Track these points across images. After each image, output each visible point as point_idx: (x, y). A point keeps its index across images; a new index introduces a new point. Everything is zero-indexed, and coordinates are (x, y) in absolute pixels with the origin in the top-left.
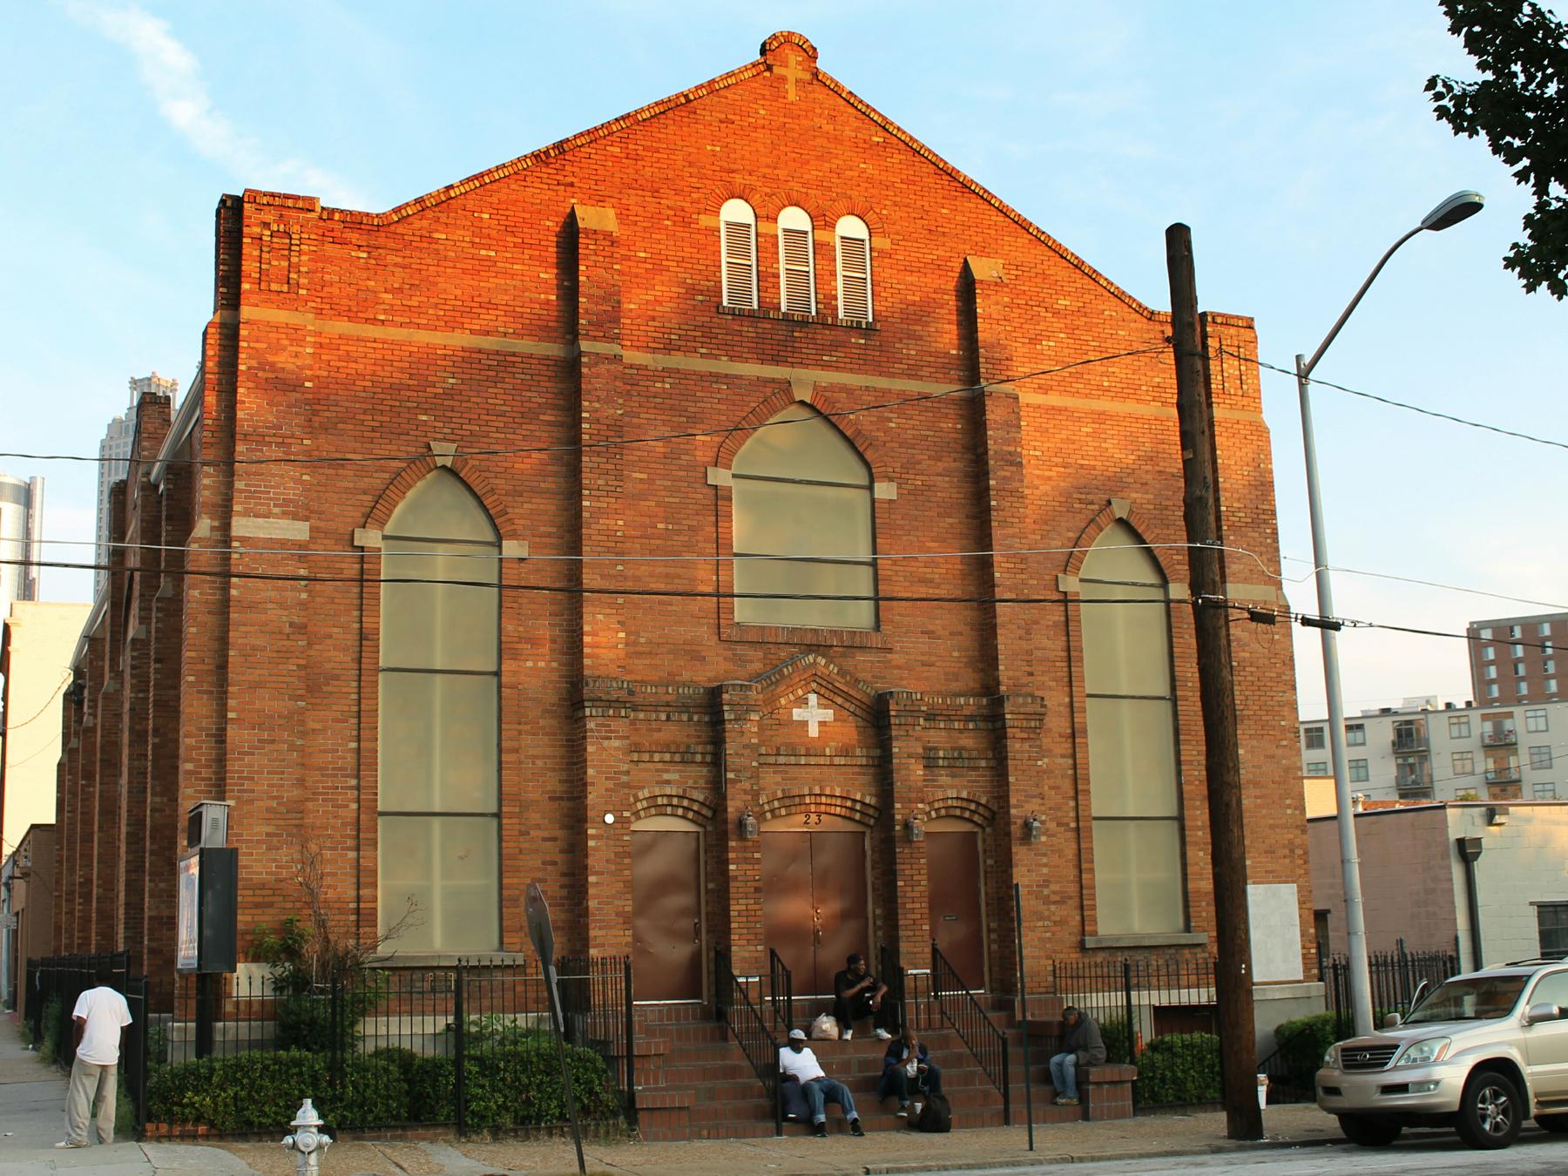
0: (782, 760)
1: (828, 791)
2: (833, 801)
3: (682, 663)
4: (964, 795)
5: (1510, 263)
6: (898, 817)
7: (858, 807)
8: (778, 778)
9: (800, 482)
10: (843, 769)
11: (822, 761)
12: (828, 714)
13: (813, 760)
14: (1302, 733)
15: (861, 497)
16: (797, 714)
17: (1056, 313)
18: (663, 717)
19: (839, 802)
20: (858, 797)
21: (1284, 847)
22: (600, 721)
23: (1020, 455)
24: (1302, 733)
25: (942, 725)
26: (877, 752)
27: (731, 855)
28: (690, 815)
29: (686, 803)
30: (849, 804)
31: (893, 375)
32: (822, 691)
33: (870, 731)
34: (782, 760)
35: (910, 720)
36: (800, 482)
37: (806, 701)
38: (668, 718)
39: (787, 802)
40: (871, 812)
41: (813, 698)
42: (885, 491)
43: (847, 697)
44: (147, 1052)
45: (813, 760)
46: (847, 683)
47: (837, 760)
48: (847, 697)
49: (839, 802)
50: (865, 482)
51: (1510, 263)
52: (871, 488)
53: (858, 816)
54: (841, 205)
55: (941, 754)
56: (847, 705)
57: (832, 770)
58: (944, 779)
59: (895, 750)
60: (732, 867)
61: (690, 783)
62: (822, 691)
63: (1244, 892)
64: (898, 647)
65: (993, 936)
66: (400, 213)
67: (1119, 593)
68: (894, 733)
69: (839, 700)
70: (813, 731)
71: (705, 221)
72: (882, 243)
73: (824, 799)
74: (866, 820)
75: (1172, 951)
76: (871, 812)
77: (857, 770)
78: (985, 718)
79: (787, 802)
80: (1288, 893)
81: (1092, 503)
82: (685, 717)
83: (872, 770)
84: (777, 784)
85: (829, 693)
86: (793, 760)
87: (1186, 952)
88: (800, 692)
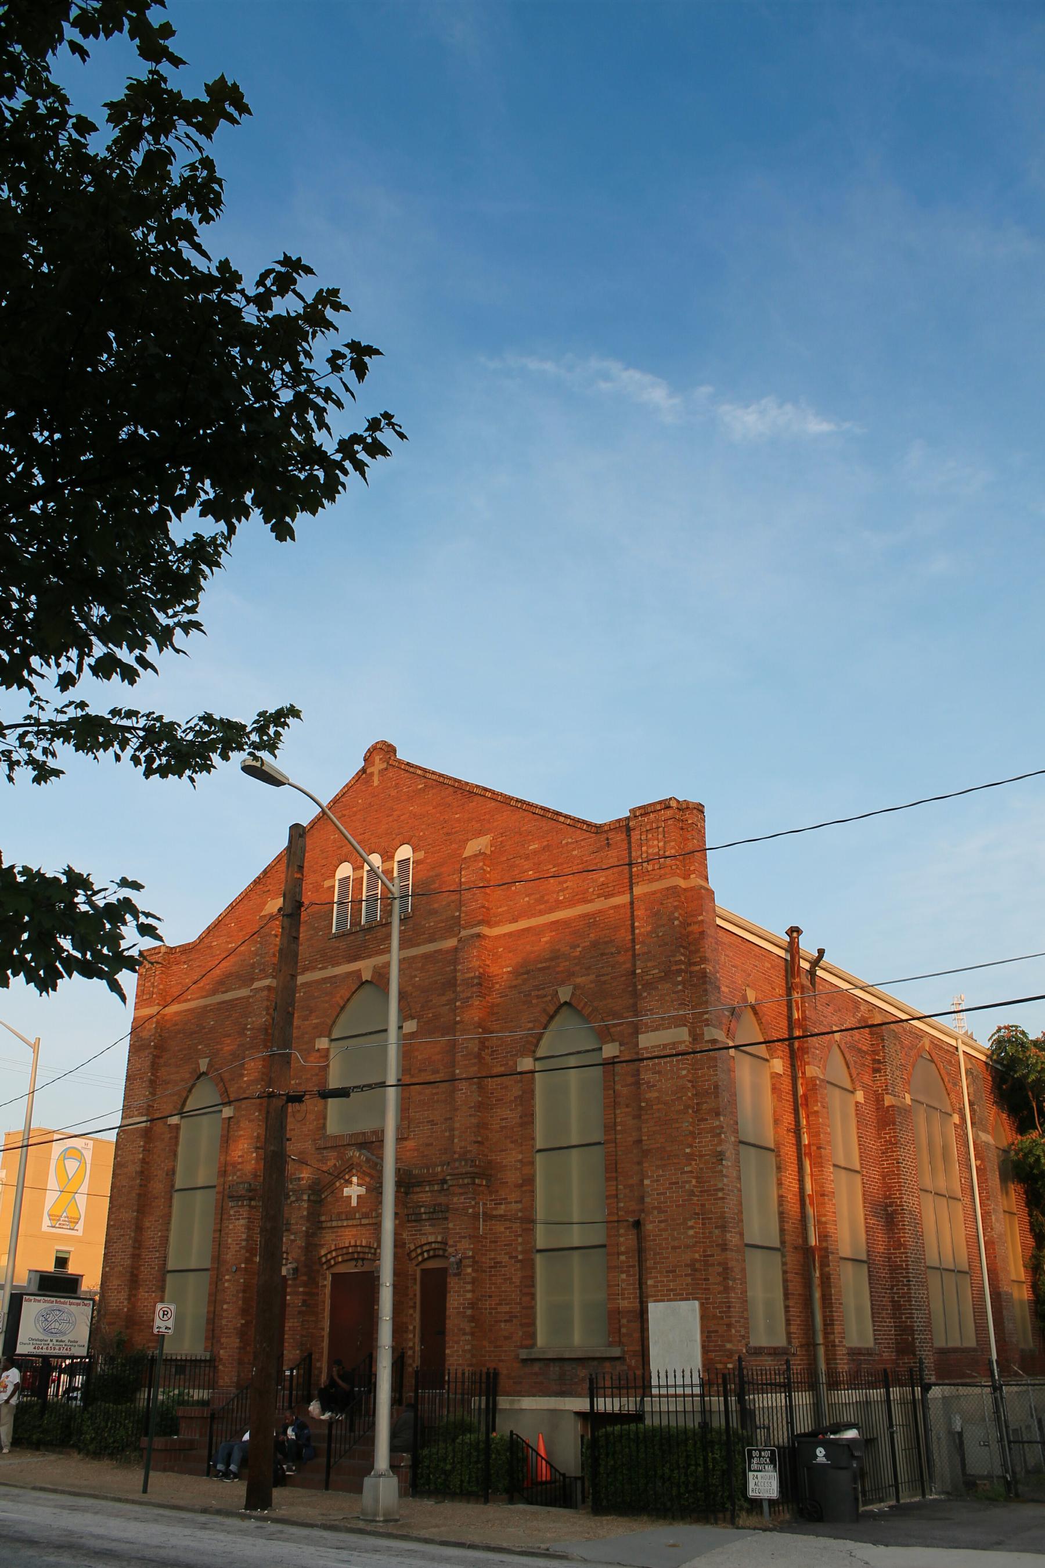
0: (334, 1224)
4: (439, 1239)
5: (147, 778)
9: (371, 1033)
10: (368, 1227)
16: (347, 1191)
17: (527, 858)
21: (687, 1265)
22: (236, 1209)
25: (427, 1189)
27: (288, 1290)
31: (418, 945)
36: (371, 1033)
37: (351, 1183)
44: (63, 1406)
51: (147, 778)
54: (397, 842)
55: (423, 1210)
58: (427, 1228)
60: (288, 1298)
63: (647, 1307)
65: (411, 1344)
66: (201, 939)
67: (572, 1061)
70: (354, 1203)
71: (327, 884)
72: (421, 855)
75: (595, 1363)
78: (1004, 1150)
80: (689, 1311)
81: (545, 996)
86: (340, 1223)
87: (607, 1364)
88: (347, 1177)
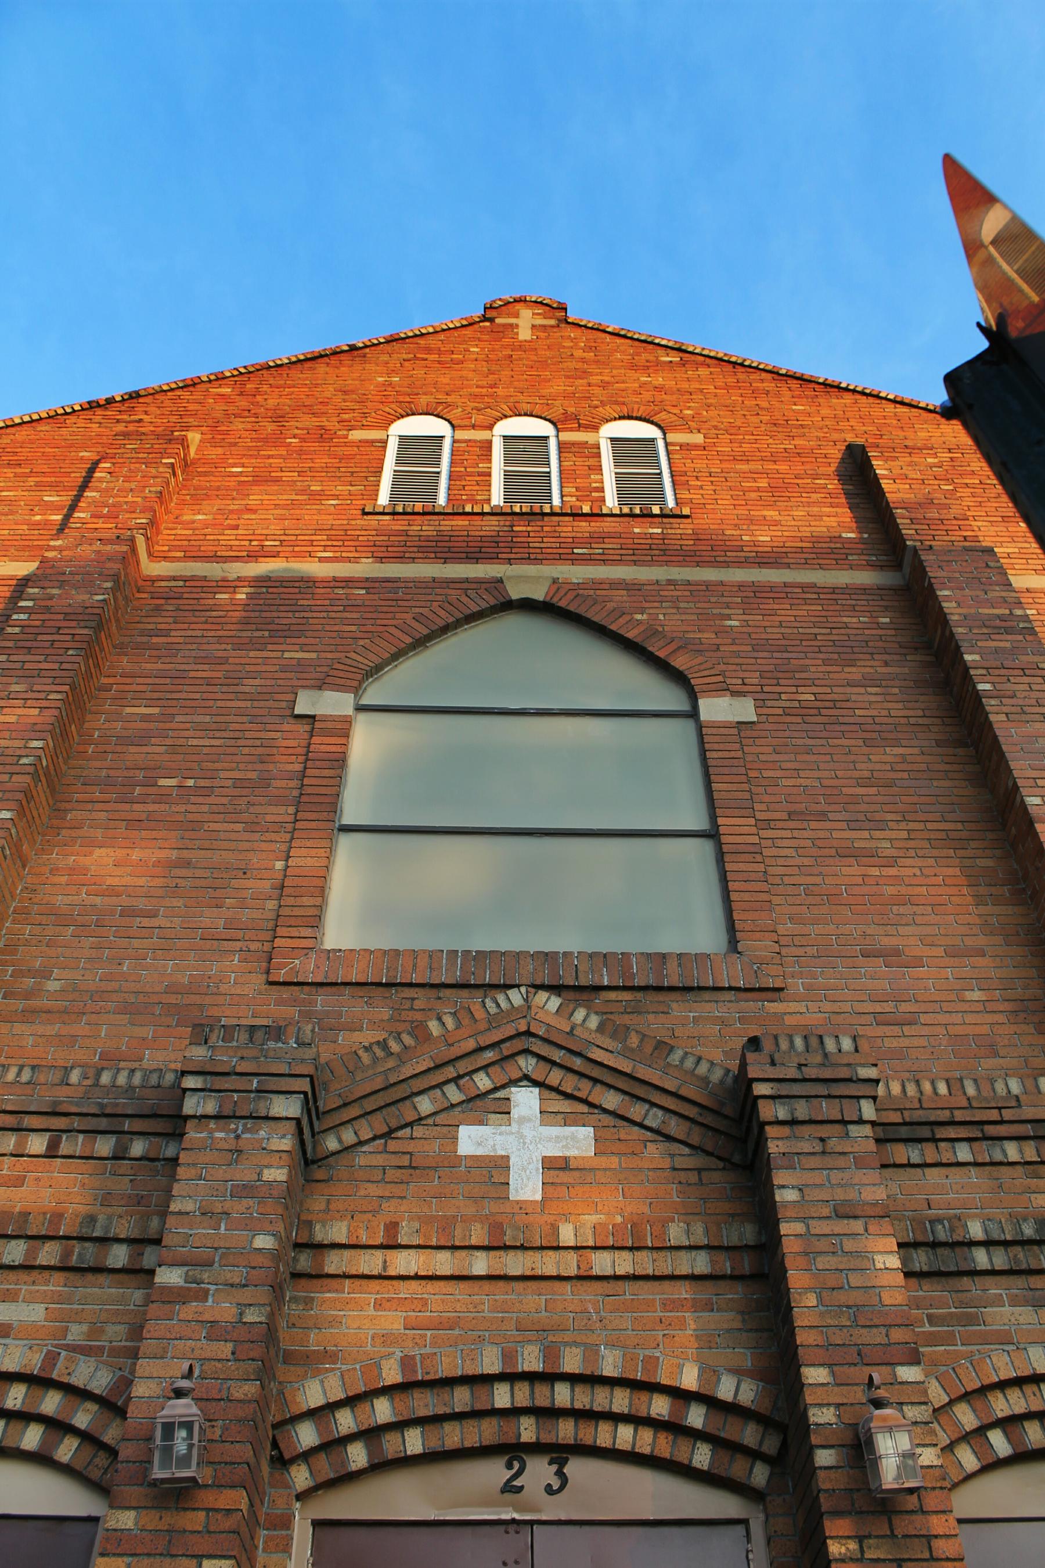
0: (404, 1262)
1: (572, 1362)
2: (600, 1399)
3: (149, 1032)
6: (821, 1416)
7: (696, 1417)
8: (393, 1321)
11: (548, 1264)
12: (578, 1141)
13: (515, 1264)
14: (481, 435)
15: (677, 736)
18: (37, 1144)
19: (620, 1401)
20: (689, 1379)
23: (1026, 618)
24: (481, 435)
26: (748, 1233)
28: (66, 1450)
29: (51, 1403)
30: (660, 1406)
32: (555, 1077)
33: (719, 1179)
34: (404, 1262)
35: (827, 1109)
38: (51, 1153)
39: (424, 1404)
40: (750, 1435)
41: (526, 1100)
42: (716, 709)
43: (633, 1087)
45: (515, 1264)
46: (626, 1053)
47: (602, 1263)
48: (633, 1087)
49: (620, 1401)
50: (685, 706)
52: (693, 714)
53: (702, 1457)
56: (637, 1111)
57: (589, 1293)
59: (786, 1196)
61: (76, 1333)
62: (555, 1077)
64: (797, 985)
68: (774, 1147)
69: (611, 1100)
73: (563, 1395)
74: (738, 1469)
76: (750, 1435)
77: (683, 1291)
79: (424, 1404)
82: (104, 1146)
83: (735, 1293)
84: (386, 1339)
85: (576, 1082)
86: (443, 1263)
